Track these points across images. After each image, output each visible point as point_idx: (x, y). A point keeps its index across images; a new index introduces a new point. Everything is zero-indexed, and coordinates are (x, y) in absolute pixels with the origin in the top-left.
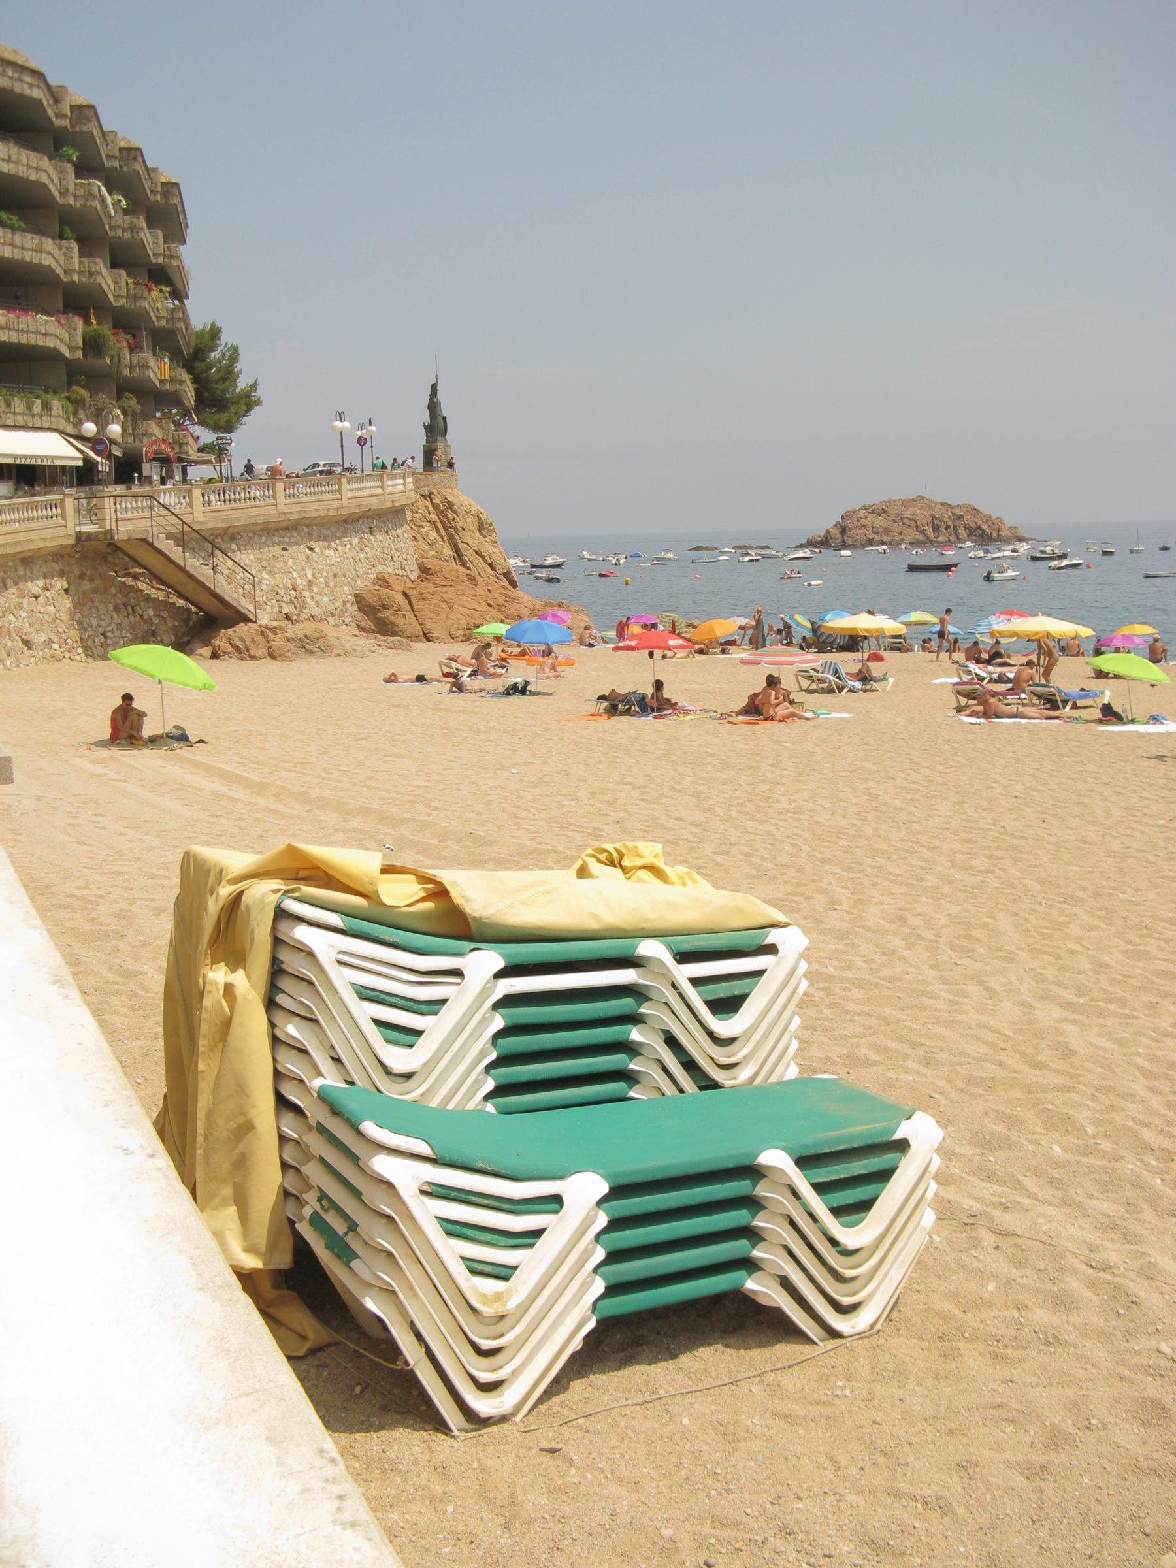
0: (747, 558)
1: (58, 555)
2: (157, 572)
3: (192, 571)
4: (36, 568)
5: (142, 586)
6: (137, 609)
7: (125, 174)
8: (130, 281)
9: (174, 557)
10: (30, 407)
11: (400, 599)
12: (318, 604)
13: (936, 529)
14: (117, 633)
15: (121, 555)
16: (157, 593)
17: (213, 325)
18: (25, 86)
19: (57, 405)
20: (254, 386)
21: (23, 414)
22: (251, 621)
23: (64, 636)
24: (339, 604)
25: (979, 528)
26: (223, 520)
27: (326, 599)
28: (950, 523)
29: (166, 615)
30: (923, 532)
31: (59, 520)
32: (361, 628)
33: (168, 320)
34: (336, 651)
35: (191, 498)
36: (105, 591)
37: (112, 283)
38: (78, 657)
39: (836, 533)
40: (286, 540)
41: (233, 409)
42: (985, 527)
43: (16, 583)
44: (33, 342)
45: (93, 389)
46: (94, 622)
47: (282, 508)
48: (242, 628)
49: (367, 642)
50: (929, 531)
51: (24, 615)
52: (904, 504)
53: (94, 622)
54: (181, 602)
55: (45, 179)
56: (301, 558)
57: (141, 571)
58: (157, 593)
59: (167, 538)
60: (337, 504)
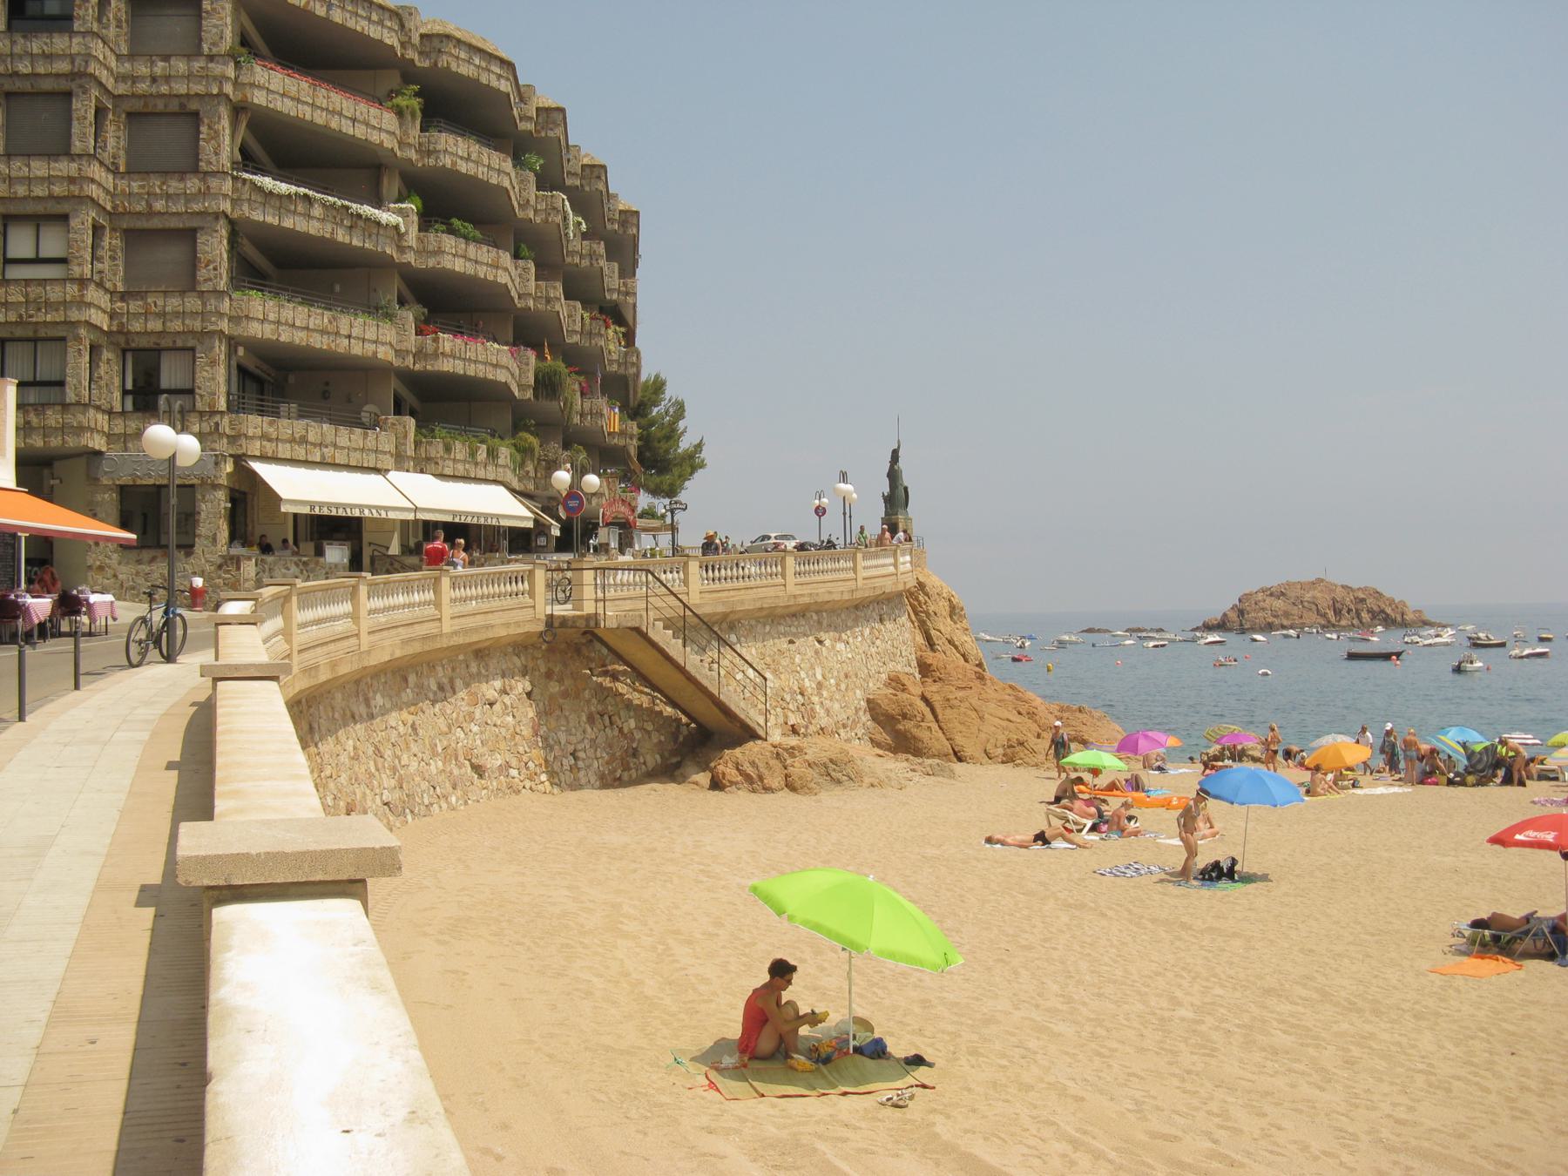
0: (1151, 644)
1: (521, 646)
2: (644, 671)
3: (693, 672)
4: (493, 663)
5: (621, 688)
6: (615, 718)
7: (589, 193)
8: (586, 315)
9: (672, 653)
10: (473, 454)
11: (921, 705)
12: (828, 711)
13: (1337, 612)
14: (591, 752)
15: (598, 645)
16: (641, 698)
17: (657, 377)
18: (493, 77)
19: (505, 452)
20: (699, 447)
21: (464, 461)
22: (759, 738)
23: (525, 758)
24: (851, 712)
25: (1383, 611)
26: (724, 603)
27: (836, 706)
29: (650, 727)
30: (1324, 616)
31: (518, 600)
32: (875, 743)
33: (619, 365)
34: (867, 780)
35: (686, 574)
36: (577, 696)
37: (572, 317)
38: (541, 787)
39: (1233, 616)
40: (793, 630)
41: (676, 471)
42: (1389, 611)
43: (467, 685)
44: (481, 375)
45: (544, 436)
46: (563, 737)
47: (792, 589)
48: (752, 748)
49: (896, 766)
50: (1331, 614)
51: (475, 729)
52: (1303, 586)
53: (563, 737)
54: (668, 710)
55: (506, 184)
56: (810, 653)
57: (622, 668)
58: (641, 698)
59: (665, 628)
60: (851, 584)
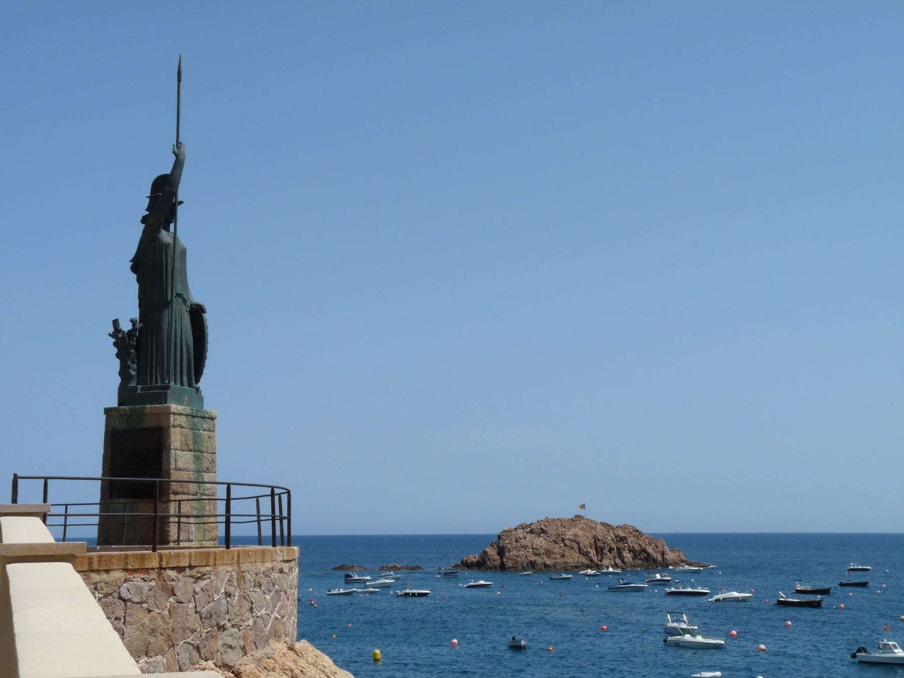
13: (599, 551)
25: (644, 550)
28: (614, 546)
30: (586, 554)
42: (650, 550)
50: (593, 552)
52: (562, 522)
